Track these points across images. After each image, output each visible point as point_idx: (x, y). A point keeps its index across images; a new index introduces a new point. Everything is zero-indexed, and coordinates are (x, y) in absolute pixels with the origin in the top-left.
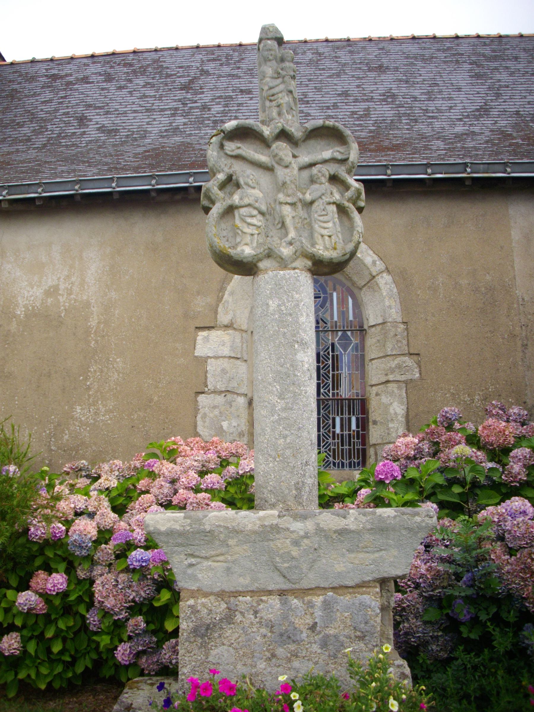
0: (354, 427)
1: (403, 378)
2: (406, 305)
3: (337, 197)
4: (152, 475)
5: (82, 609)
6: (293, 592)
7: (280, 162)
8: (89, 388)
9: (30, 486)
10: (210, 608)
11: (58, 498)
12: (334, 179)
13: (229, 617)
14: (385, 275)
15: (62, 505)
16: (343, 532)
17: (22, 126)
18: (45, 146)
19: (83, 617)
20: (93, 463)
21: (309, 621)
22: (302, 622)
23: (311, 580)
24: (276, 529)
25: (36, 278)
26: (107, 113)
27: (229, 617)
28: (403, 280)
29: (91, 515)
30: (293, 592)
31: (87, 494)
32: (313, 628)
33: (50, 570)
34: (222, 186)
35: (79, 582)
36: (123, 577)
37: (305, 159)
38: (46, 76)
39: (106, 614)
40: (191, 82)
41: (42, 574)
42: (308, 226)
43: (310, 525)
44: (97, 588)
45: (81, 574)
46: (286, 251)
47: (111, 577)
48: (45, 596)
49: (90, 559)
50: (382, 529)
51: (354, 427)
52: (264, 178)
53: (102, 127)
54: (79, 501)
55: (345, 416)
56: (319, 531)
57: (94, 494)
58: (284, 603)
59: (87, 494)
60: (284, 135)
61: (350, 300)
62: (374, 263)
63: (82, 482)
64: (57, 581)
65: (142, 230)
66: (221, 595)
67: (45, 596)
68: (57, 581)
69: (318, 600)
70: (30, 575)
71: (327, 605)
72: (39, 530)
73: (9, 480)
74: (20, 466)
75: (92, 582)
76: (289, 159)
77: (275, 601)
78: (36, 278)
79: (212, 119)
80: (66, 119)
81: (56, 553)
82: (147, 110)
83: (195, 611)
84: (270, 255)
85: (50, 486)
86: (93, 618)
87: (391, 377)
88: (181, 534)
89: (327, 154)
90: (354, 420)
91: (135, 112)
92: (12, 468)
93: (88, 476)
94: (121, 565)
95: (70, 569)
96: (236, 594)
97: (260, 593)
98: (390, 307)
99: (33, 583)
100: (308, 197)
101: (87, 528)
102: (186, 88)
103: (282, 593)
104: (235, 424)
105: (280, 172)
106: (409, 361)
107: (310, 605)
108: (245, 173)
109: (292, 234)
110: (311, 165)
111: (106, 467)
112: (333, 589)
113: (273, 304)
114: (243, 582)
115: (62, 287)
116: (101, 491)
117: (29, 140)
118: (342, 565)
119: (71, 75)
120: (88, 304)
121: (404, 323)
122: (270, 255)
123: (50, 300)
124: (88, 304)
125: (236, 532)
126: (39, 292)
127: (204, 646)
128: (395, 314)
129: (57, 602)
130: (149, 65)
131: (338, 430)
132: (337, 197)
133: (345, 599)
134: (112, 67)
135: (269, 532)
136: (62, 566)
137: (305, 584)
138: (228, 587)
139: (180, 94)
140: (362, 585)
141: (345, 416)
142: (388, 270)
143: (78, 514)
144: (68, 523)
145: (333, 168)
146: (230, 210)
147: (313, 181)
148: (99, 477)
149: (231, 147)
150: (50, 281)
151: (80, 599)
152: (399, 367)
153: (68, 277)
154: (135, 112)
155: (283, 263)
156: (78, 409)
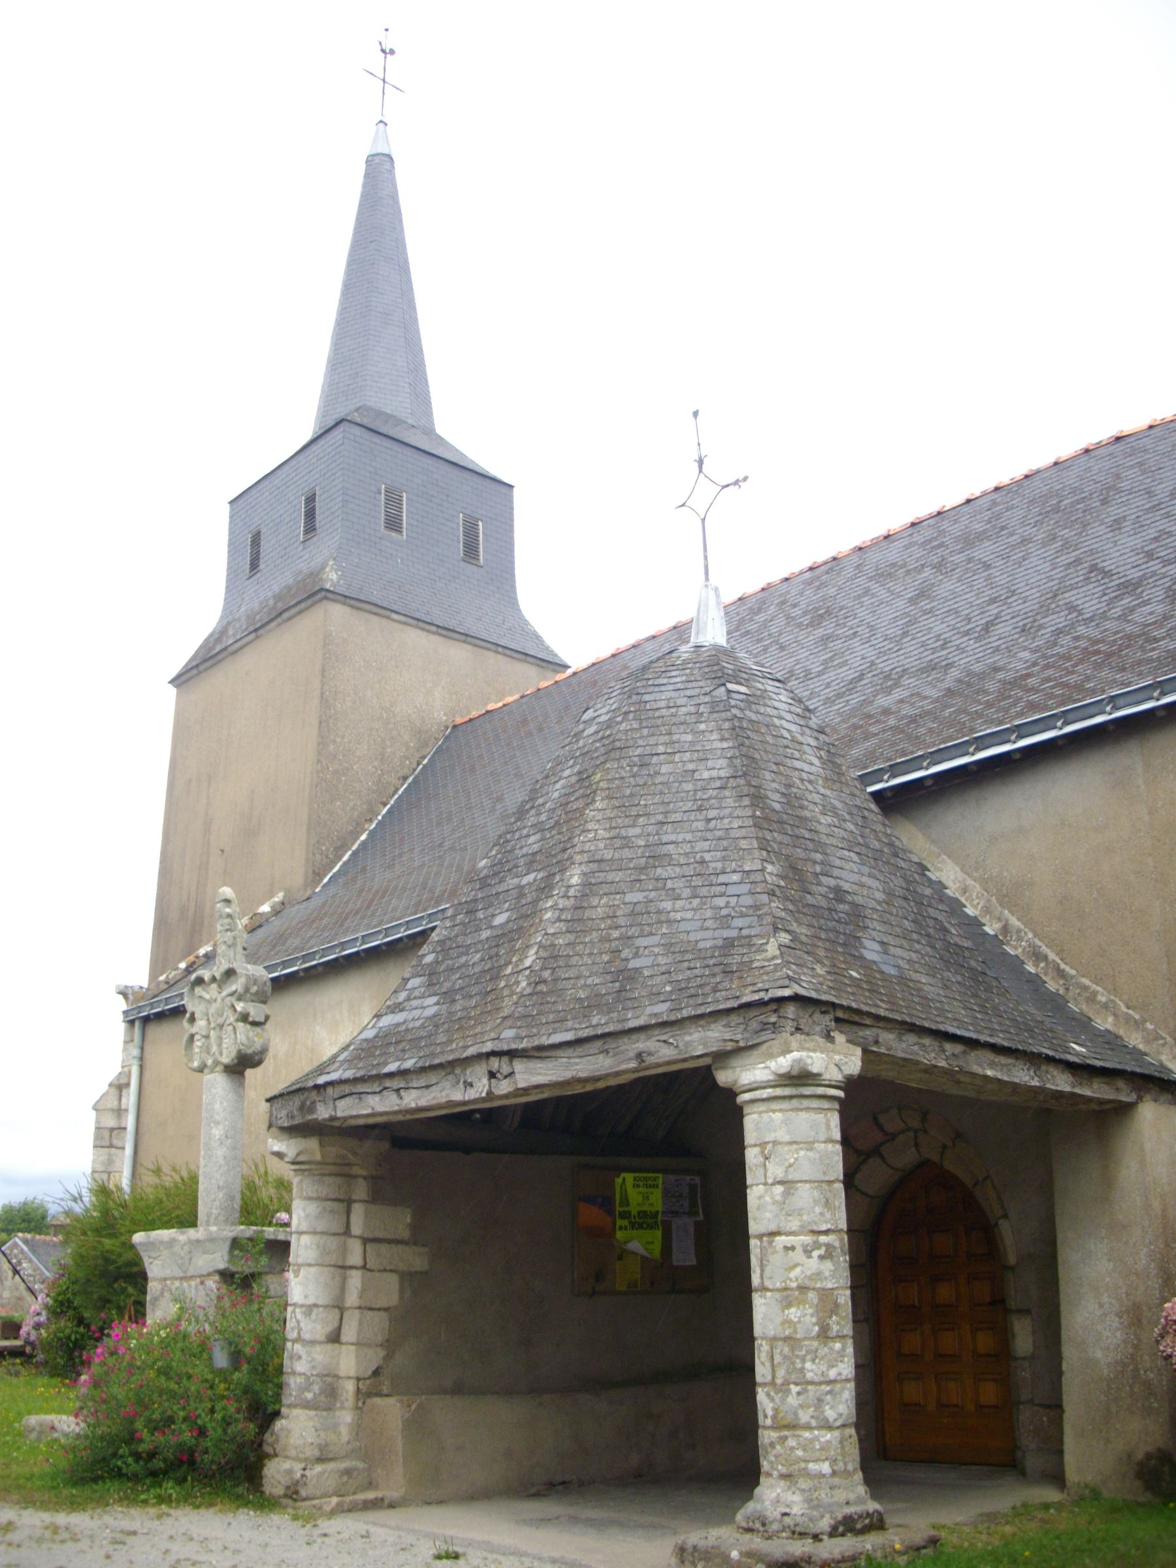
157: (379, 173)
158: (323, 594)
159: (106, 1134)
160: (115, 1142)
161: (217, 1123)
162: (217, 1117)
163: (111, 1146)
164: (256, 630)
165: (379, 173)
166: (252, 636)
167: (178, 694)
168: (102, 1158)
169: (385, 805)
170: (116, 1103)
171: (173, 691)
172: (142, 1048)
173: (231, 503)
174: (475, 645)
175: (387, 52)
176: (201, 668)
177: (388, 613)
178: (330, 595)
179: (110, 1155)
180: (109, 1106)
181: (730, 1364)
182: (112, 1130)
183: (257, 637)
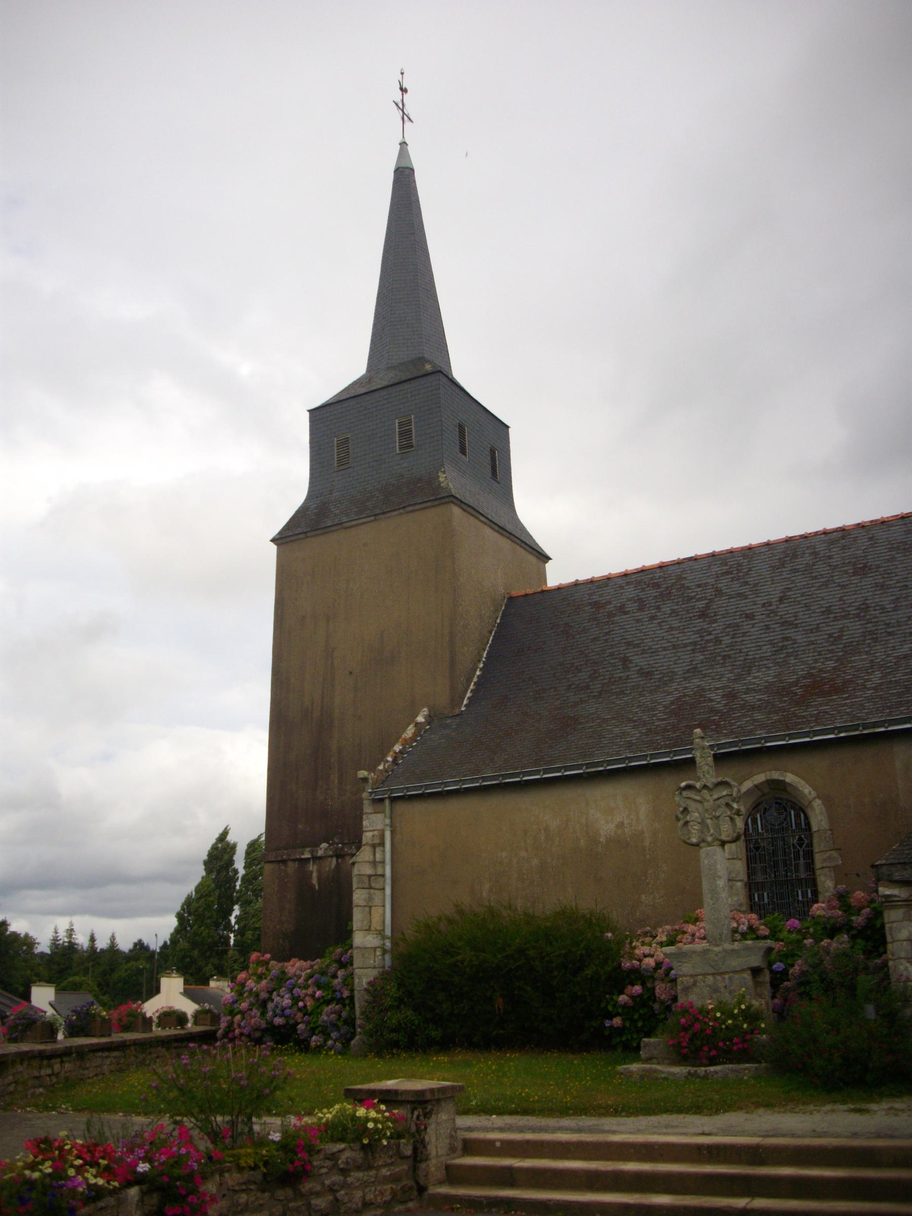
0: (810, 896)
1: (832, 864)
2: (831, 818)
3: (729, 813)
4: (684, 933)
5: (651, 1003)
6: (717, 974)
7: (705, 799)
8: (648, 884)
9: (620, 943)
10: (688, 981)
11: (635, 948)
12: (727, 805)
13: (695, 984)
14: (817, 800)
15: (637, 951)
16: (733, 950)
17: (580, 671)
18: (600, 693)
19: (652, 1007)
20: (655, 928)
21: (724, 984)
22: (721, 985)
23: (724, 969)
24: (708, 950)
25: (610, 818)
26: (644, 652)
27: (695, 984)
28: (828, 801)
29: (652, 956)
30: (717, 974)
31: (650, 946)
32: (725, 987)
33: (633, 985)
34: (682, 812)
35: (648, 989)
36: (669, 984)
37: (715, 797)
38: (590, 604)
39: (662, 1002)
40: (707, 607)
41: (629, 987)
42: (717, 827)
43: (720, 948)
44: (657, 991)
45: (649, 985)
46: (709, 839)
47: (663, 985)
48: (632, 997)
49: (652, 977)
50: (747, 948)
51: (810, 896)
52: (699, 806)
53: (641, 669)
54: (646, 950)
55: (804, 889)
56: (724, 950)
57: (654, 945)
58: (714, 978)
59: (650, 946)
60: (705, 787)
61: (802, 815)
62: (810, 793)
63: (648, 940)
64: (637, 989)
65: (669, 782)
66: (691, 976)
67: (632, 997)
68: (637, 989)
69: (727, 976)
70: (624, 988)
71: (730, 978)
72: (627, 964)
73: (609, 941)
74: (613, 933)
75: (654, 989)
76: (708, 798)
77: (711, 978)
78: (610, 818)
79: (723, 654)
80: (612, 661)
81: (636, 975)
82: (674, 647)
83: (682, 982)
84: (703, 841)
85: (631, 943)
86: (656, 1006)
87: (824, 865)
88: (675, 954)
89: (724, 793)
90: (809, 891)
91: (665, 649)
92: (610, 935)
93: (651, 936)
94: (667, 980)
95: (643, 984)
96: (697, 975)
97: (705, 975)
98: (821, 820)
99: (625, 991)
100: (717, 814)
101: (650, 962)
102: (703, 615)
103: (713, 974)
104: (735, 899)
105: (706, 804)
106: (834, 853)
107: (724, 978)
108: (692, 806)
109: (712, 831)
110: (718, 799)
111: (660, 930)
112: (733, 972)
113: (706, 862)
114: (699, 971)
115: (626, 822)
116: (657, 944)
117: (588, 687)
118: (735, 963)
119: (610, 603)
120: (642, 832)
121: (830, 830)
122: (703, 841)
123: (619, 831)
124: (642, 832)
125: (694, 952)
126: (612, 826)
127: (686, 995)
128: (825, 825)
129: (638, 1000)
130: (673, 585)
131: (800, 898)
132: (729, 813)
133: (737, 976)
134: (643, 590)
135: (706, 952)
136: (639, 982)
137: (721, 971)
138: (694, 973)
139: (699, 623)
140: (743, 971)
141: (804, 889)
142: (818, 797)
143: (645, 956)
144: (640, 960)
145: (727, 799)
146: (686, 823)
147: (719, 806)
148: (657, 936)
149: (685, 793)
150: (618, 819)
151: (649, 998)
152: (829, 857)
153: (629, 816)
154: (665, 649)
155: (709, 845)
156: (643, 896)
157: (404, 180)
158: (452, 499)
159: (366, 880)
160: (373, 885)
161: (720, 877)
162: (720, 874)
163: (370, 888)
164: (375, 515)
165: (404, 180)
166: (372, 518)
167: (278, 549)
168: (363, 896)
169: (484, 650)
170: (372, 857)
171: (274, 548)
172: (391, 818)
173: (311, 412)
174: (513, 541)
175: (404, 90)
176: (309, 534)
177: (478, 515)
178: (455, 500)
179: (369, 894)
180: (367, 859)
181: (78, 1036)
182: (370, 876)
183: (375, 520)
